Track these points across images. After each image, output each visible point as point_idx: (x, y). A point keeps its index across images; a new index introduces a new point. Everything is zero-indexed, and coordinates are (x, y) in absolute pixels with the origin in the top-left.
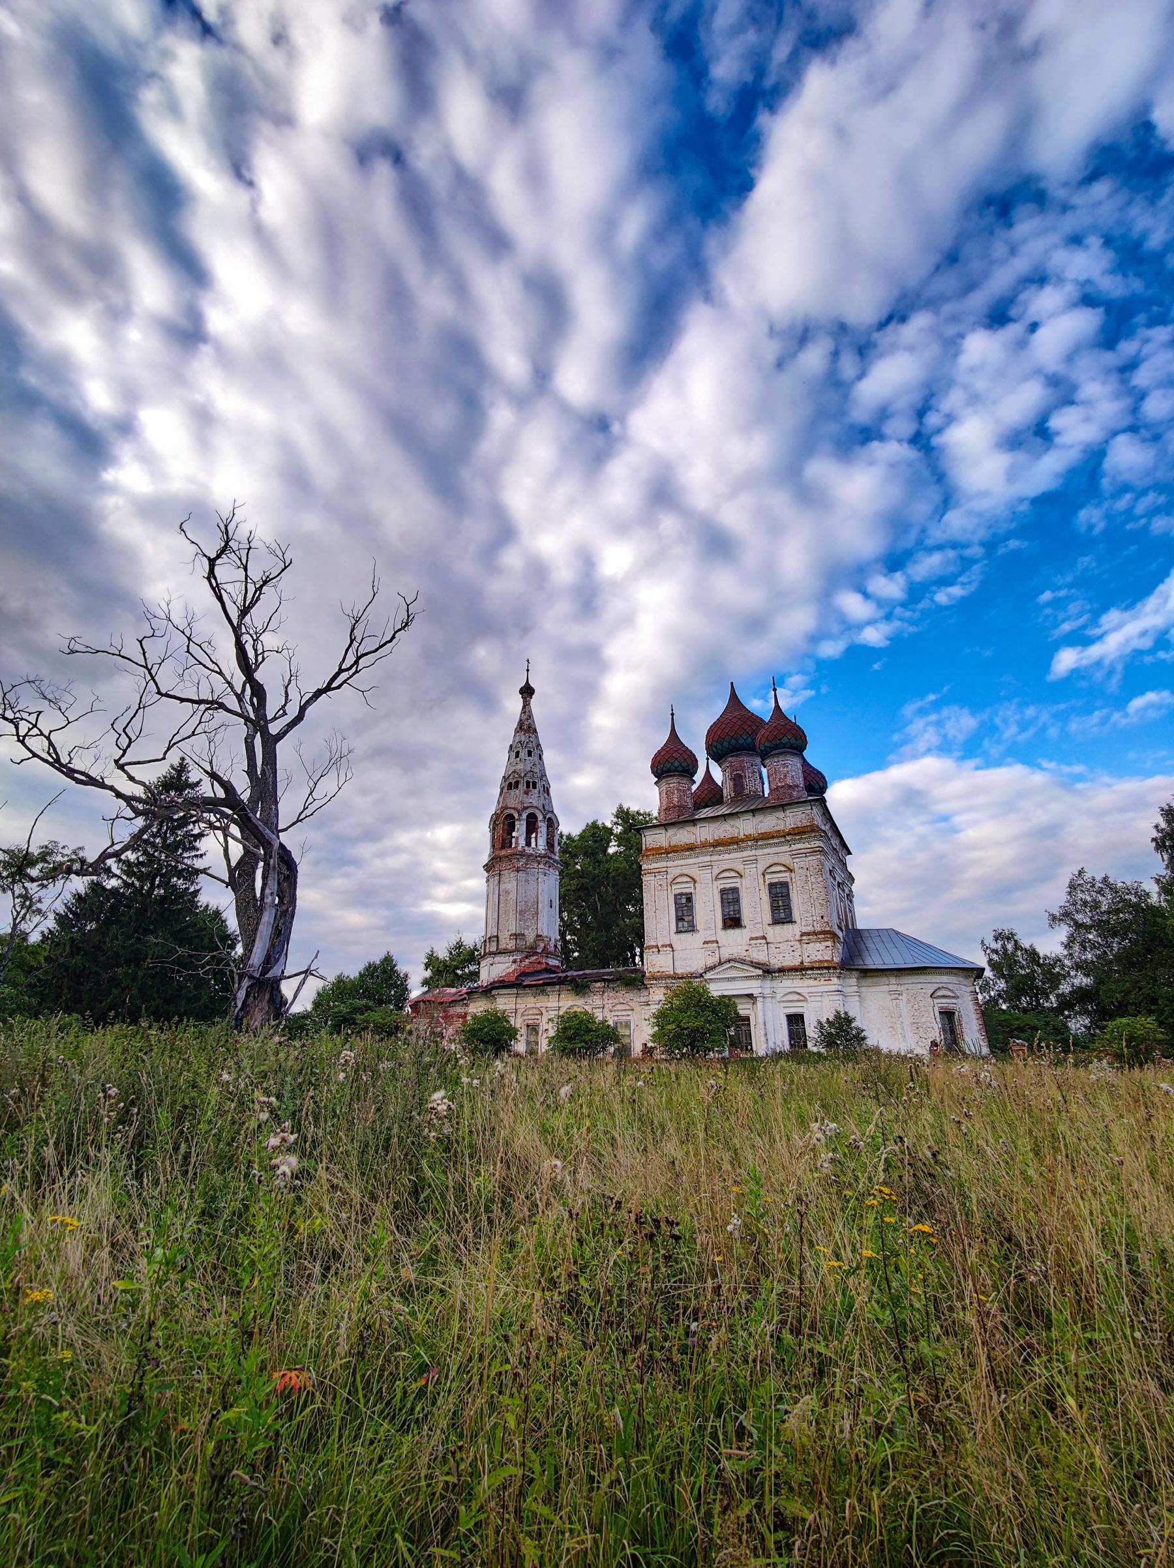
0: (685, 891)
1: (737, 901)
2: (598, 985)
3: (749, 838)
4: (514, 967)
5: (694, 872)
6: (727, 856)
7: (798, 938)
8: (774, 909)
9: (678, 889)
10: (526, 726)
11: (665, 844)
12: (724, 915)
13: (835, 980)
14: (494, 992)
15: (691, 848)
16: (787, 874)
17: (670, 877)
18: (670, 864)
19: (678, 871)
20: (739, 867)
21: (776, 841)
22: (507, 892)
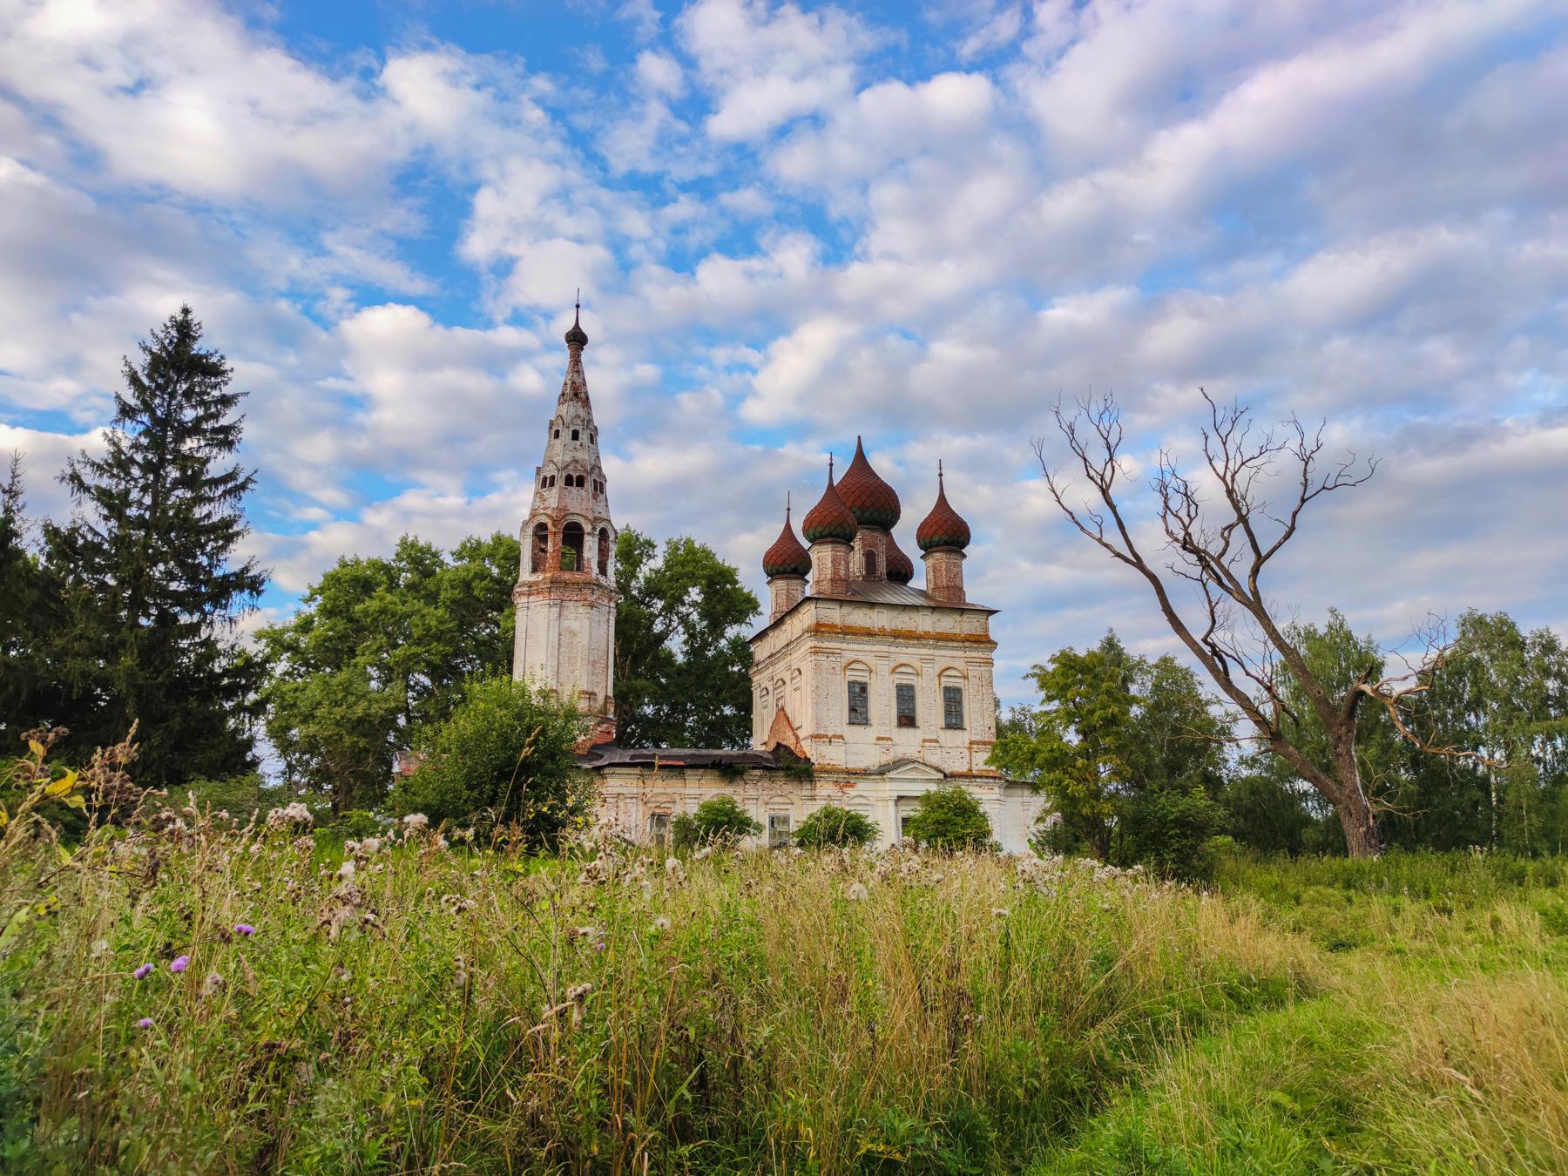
0: (859, 679)
1: (912, 699)
2: (757, 772)
5: (870, 659)
6: (904, 650)
7: (967, 745)
8: (948, 713)
11: (838, 621)
12: (899, 712)
13: (996, 790)
15: (869, 634)
16: (961, 680)
17: (844, 661)
18: (844, 646)
19: (851, 656)
20: (917, 664)
21: (955, 644)
22: (573, 633)
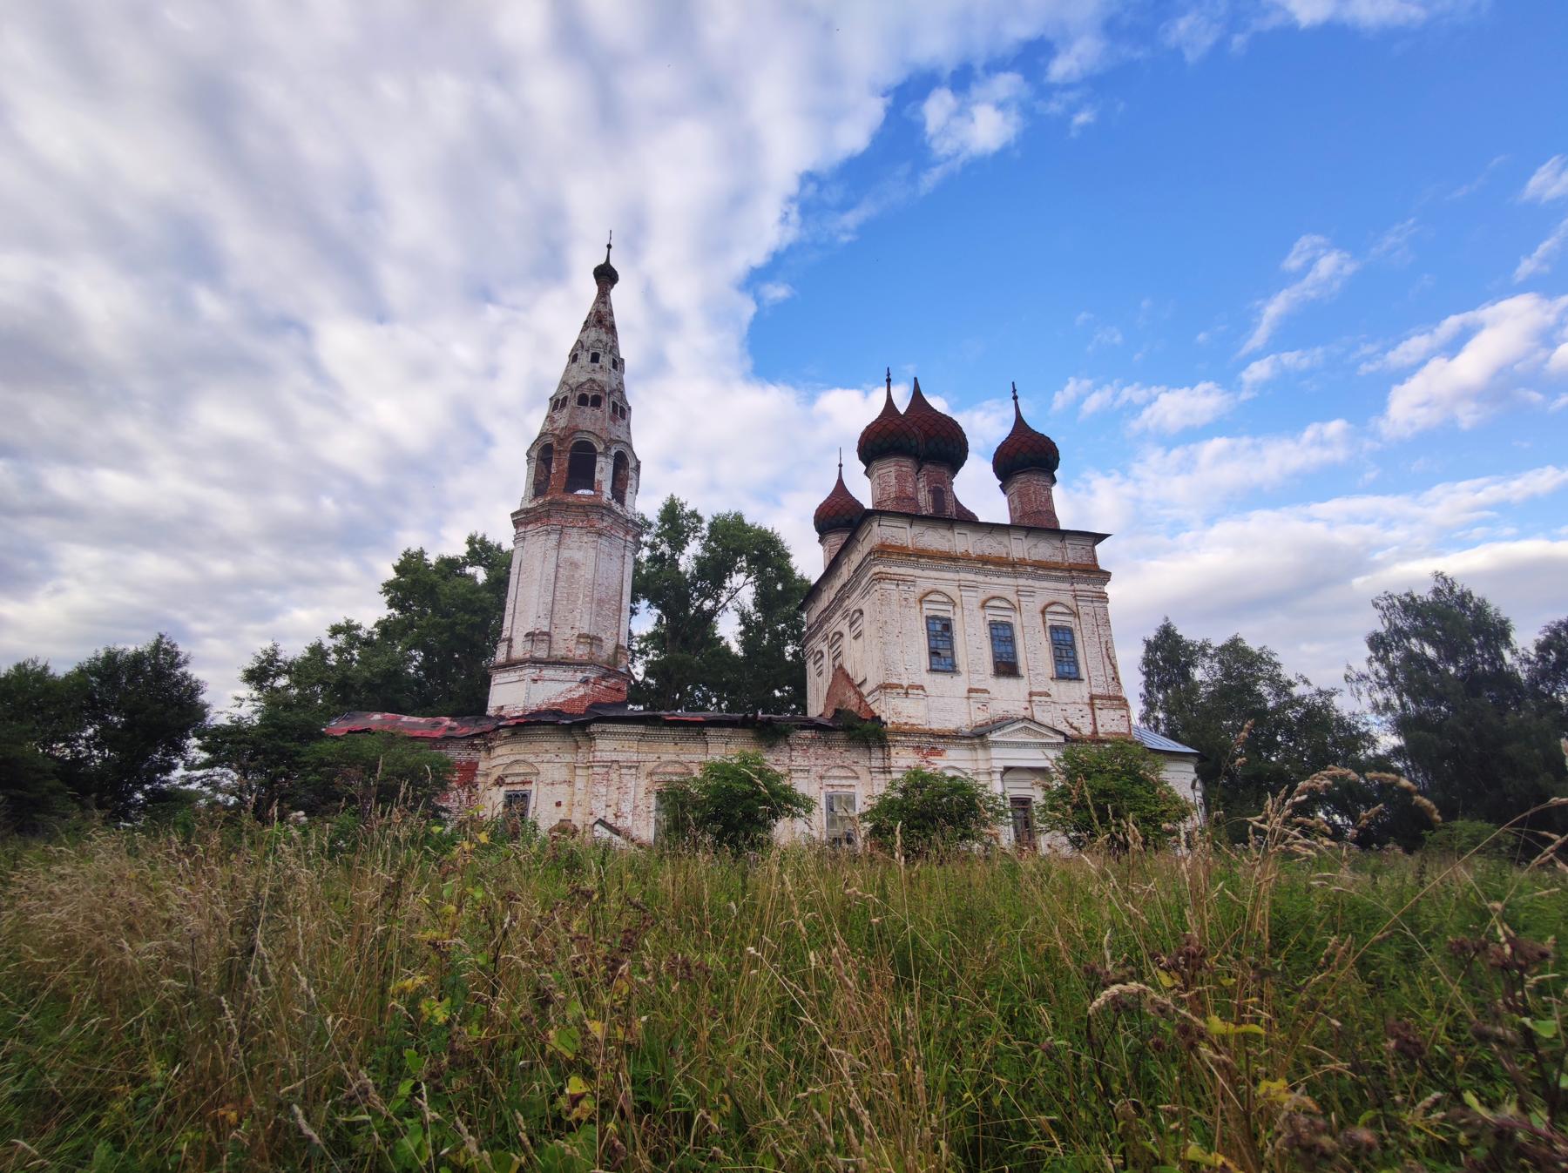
3: (1022, 562)
4: (581, 691)
6: (995, 580)
8: (1058, 660)
9: (930, 609)
10: (601, 319)
12: (995, 656)
14: (594, 728)
16: (1071, 619)
18: (918, 572)
19: (929, 585)
20: (953, 591)
